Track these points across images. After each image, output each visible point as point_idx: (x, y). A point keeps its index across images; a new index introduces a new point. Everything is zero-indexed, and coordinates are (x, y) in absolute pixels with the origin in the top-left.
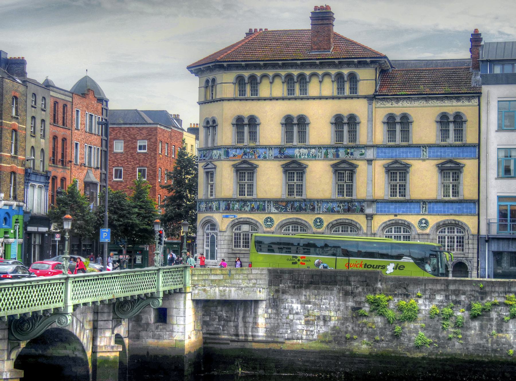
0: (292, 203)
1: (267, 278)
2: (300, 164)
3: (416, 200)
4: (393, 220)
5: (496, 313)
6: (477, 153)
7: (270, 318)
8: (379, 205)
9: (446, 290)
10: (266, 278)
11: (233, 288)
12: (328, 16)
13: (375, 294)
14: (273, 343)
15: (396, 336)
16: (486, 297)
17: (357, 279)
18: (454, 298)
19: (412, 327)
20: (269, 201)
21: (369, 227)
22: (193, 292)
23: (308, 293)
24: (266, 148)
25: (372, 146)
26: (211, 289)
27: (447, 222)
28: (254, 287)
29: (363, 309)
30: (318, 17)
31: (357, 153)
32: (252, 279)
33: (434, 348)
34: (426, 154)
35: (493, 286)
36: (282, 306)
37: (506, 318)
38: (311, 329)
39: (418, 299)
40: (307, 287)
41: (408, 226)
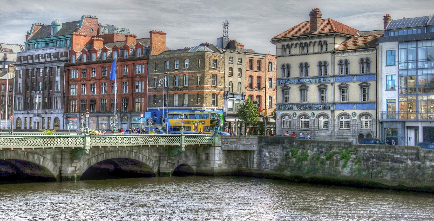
1: (257, 140)
6: (376, 78)
8: (337, 106)
15: (299, 168)
16: (332, 149)
20: (294, 104)
21: (333, 116)
31: (327, 80)
37: (339, 160)
41: (348, 115)
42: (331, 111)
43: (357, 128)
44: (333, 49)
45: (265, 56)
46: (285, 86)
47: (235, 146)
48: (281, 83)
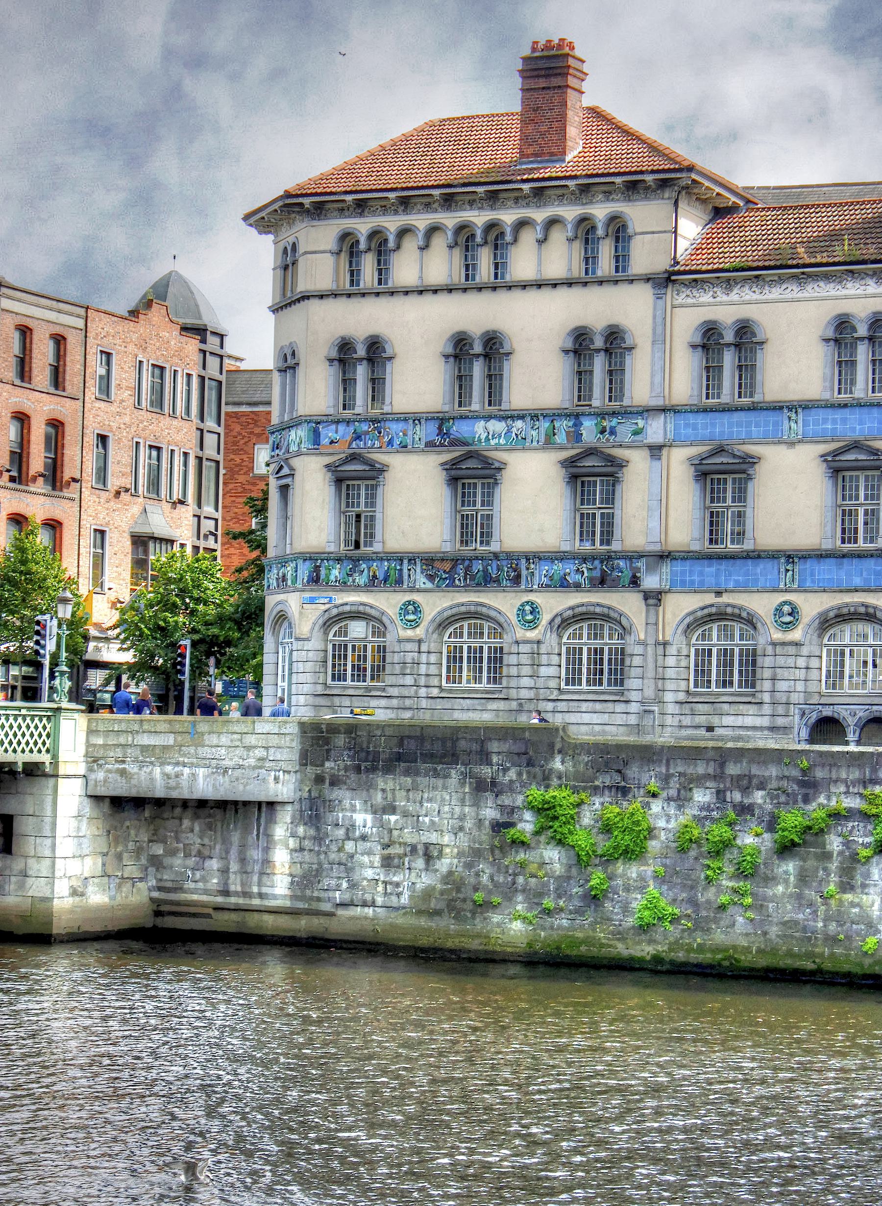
0: (467, 563)
1: (296, 745)
2: (487, 463)
3: (768, 551)
4: (712, 606)
5: (840, 839)
7: (302, 849)
8: (678, 567)
9: (719, 777)
10: (294, 744)
11: (202, 770)
12: (561, 64)
13: (547, 787)
14: (307, 914)
17: (505, 747)
18: (737, 796)
19: (634, 875)
21: (653, 624)
22: (92, 776)
23: (390, 785)
24: (406, 420)
25: (664, 410)
26: (141, 768)
27: (845, 611)
28: (261, 767)
29: (520, 826)
30: (536, 70)
31: (624, 431)
32: (255, 747)
33: (683, 931)
34: (797, 428)
35: (835, 765)
36: (330, 818)
37: (865, 853)
38: (396, 879)
39: (650, 800)
40: (388, 769)
41: (750, 621)
42: (646, 598)
43: (800, 686)
44: (662, 264)
45: (82, 312)
46: (353, 458)
47: (168, 776)
48: (325, 441)
